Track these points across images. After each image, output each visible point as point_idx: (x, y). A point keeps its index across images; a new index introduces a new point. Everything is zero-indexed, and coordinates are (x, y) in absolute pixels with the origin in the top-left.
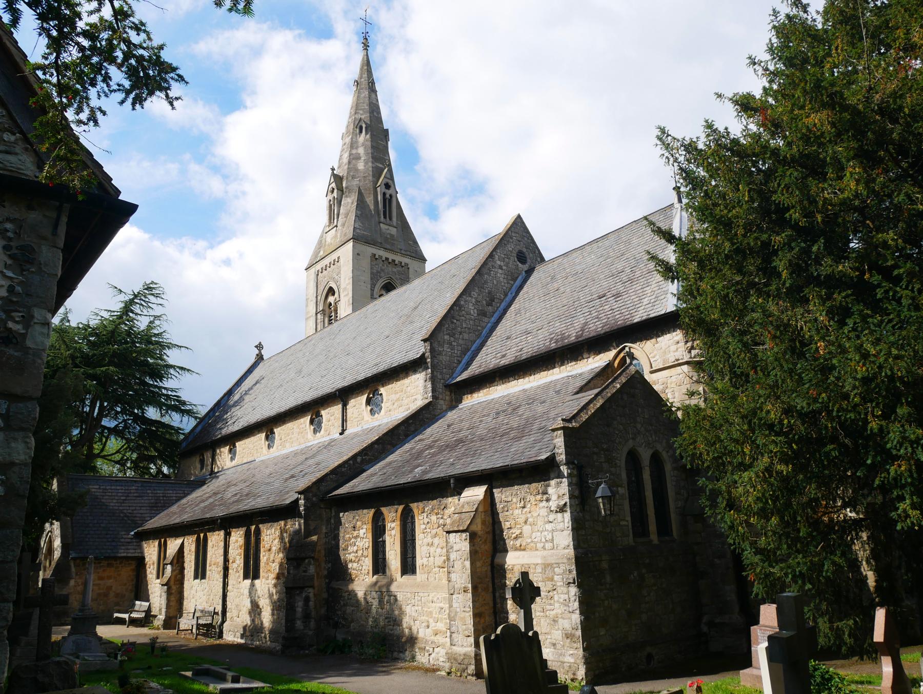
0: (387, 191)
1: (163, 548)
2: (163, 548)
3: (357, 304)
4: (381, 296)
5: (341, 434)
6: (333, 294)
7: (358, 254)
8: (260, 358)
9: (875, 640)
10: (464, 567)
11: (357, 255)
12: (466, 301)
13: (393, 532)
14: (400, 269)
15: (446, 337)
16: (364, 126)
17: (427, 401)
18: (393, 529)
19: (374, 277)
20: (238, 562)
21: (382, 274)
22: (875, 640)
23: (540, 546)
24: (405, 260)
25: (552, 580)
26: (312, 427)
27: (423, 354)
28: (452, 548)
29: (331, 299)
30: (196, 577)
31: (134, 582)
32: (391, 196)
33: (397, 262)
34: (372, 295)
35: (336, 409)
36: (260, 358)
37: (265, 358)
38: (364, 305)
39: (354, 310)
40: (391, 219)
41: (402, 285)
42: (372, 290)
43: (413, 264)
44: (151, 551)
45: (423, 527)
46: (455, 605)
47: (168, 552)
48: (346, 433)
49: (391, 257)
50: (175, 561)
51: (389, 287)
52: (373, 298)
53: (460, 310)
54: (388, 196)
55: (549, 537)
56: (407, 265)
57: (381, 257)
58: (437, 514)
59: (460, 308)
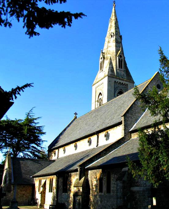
0: (120, 58)
1: (40, 181)
2: (40, 181)
3: (109, 98)
4: (118, 96)
5: (97, 146)
6: (101, 95)
7: (110, 81)
8: (76, 118)
9: (154, 205)
10: (120, 191)
11: (109, 82)
12: (137, 103)
13: (105, 180)
14: (125, 86)
15: (130, 115)
16: (113, 35)
17: (122, 137)
18: (105, 179)
19: (115, 89)
20: (61, 187)
21: (118, 88)
22: (154, 205)
23: (142, 185)
24: (126, 83)
25: (145, 195)
26: (105, 138)
27: (122, 121)
28: (118, 185)
29: (100, 97)
30: (50, 192)
31: (31, 193)
32: (122, 60)
33: (124, 84)
34: (114, 95)
35: (96, 136)
36: (76, 118)
37: (77, 117)
38: (111, 99)
39: (108, 101)
40: (122, 68)
41: (125, 92)
42: (114, 94)
43: (130, 85)
44: (37, 183)
45: (113, 178)
46: (118, 202)
47: (42, 184)
48: (98, 146)
49: (122, 82)
50: (43, 186)
51: (121, 93)
52: (115, 97)
53: (135, 106)
54: (121, 60)
55: (145, 183)
56: (127, 84)
57: (118, 82)
58: (116, 175)
59: (135, 105)
